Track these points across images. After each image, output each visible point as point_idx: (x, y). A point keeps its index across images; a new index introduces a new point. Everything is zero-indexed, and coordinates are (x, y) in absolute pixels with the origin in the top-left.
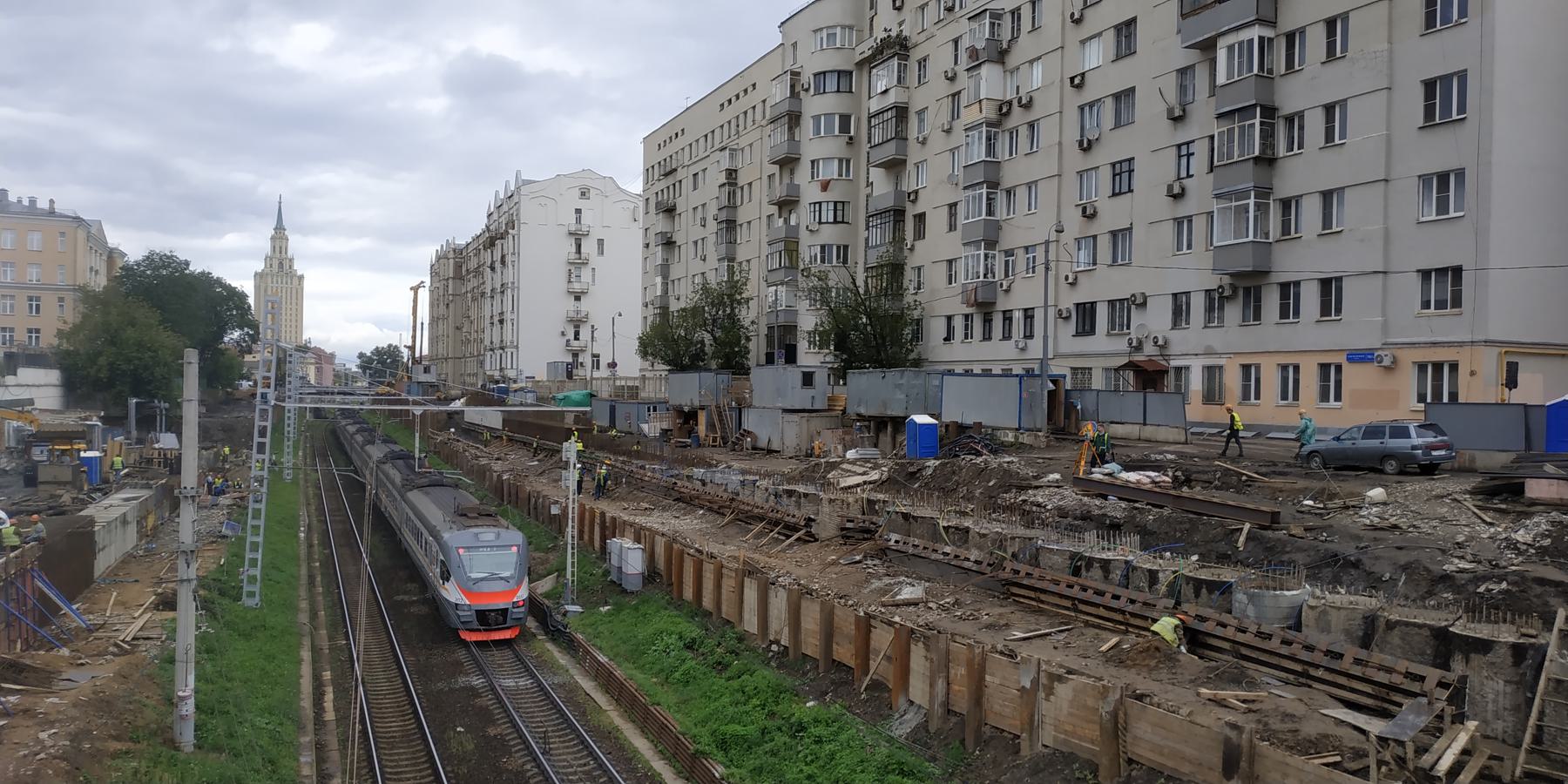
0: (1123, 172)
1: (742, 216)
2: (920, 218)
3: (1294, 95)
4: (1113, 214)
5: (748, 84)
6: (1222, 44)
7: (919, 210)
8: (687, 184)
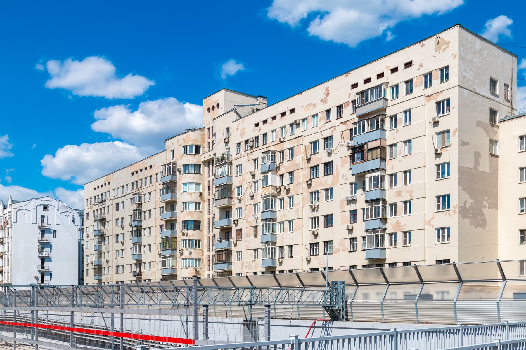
0: (329, 220)
1: (145, 224)
2: (240, 231)
3: (390, 196)
4: (324, 234)
5: (287, 110)
6: (367, 177)
7: (239, 227)
8: (113, 208)
